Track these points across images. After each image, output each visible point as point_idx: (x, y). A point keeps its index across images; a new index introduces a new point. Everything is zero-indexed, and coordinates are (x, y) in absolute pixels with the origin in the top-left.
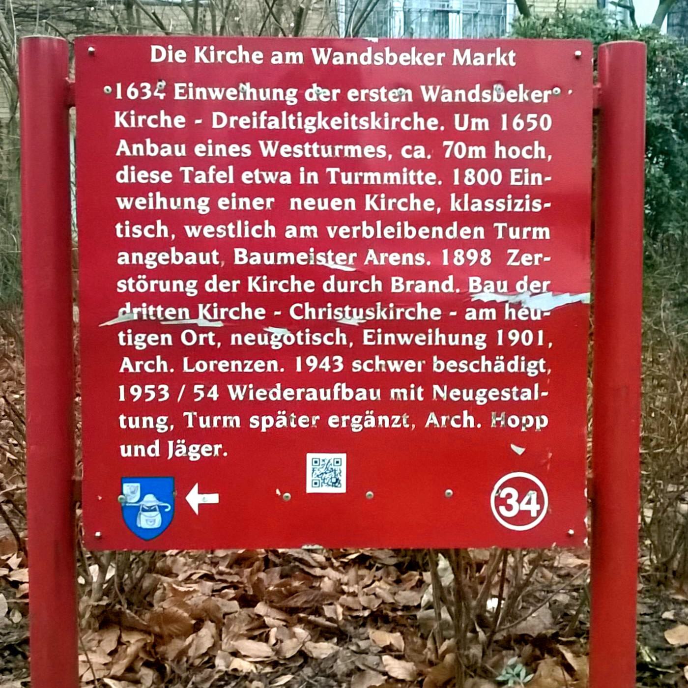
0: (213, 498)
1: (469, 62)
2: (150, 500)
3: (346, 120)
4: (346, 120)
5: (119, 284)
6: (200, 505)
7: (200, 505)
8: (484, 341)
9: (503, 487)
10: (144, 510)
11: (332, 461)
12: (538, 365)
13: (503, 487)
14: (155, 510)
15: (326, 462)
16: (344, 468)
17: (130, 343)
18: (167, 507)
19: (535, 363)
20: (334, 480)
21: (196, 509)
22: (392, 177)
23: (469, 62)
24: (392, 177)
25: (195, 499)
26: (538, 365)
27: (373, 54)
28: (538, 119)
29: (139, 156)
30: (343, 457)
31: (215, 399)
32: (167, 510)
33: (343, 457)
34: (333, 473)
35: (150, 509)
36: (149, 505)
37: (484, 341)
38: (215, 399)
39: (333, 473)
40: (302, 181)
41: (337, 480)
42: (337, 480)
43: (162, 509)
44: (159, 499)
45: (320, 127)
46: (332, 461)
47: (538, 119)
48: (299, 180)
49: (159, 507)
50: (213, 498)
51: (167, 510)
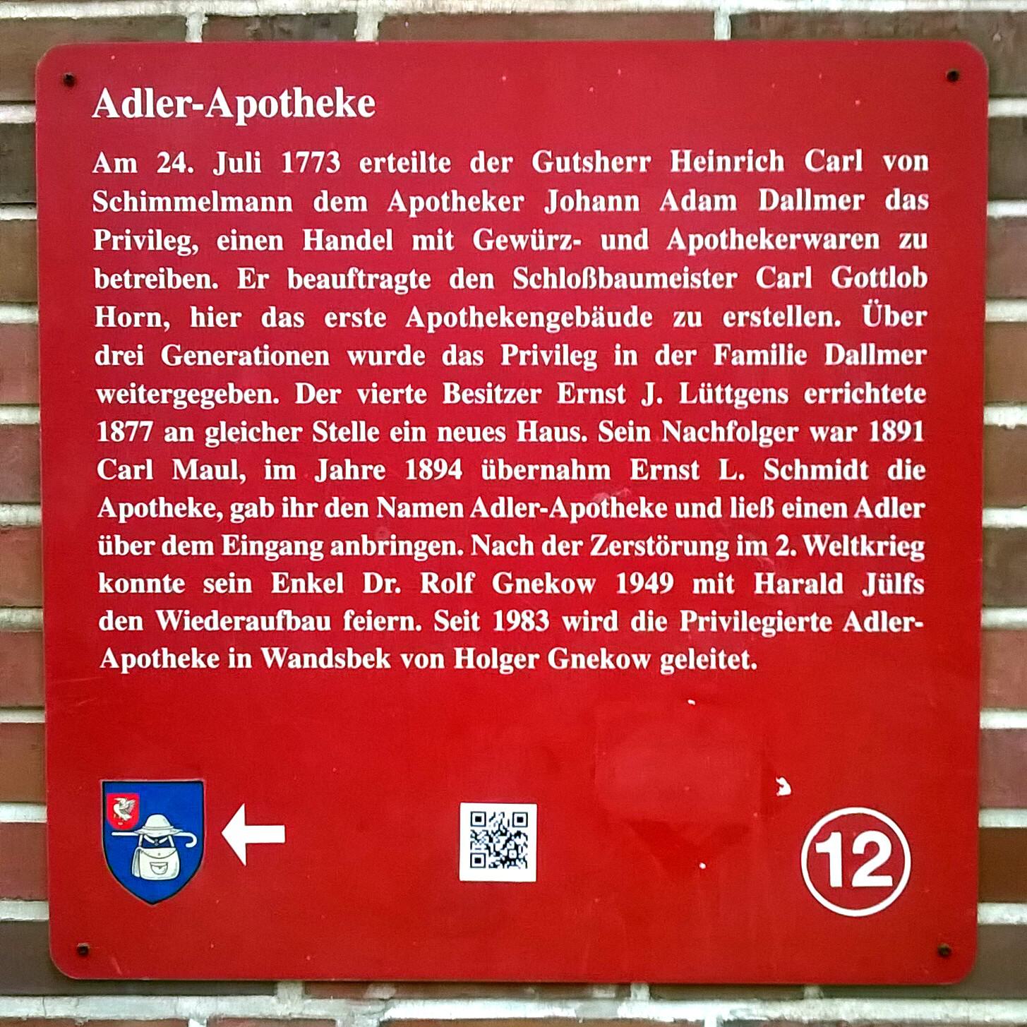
0: (274, 834)
1: (194, 476)
2: (157, 825)
3: (713, 657)
4: (713, 657)
5: (926, 204)
6: (250, 848)
7: (250, 848)
9: (886, 892)
10: (146, 845)
13: (886, 892)
14: (167, 845)
16: (531, 830)
18: (190, 840)
21: (242, 855)
23: (194, 476)
25: (240, 834)
27: (334, 655)
29: (868, 343)
30: (531, 810)
31: (458, 477)
32: (189, 845)
33: (531, 810)
35: (159, 843)
36: (156, 834)
38: (458, 477)
40: (232, 665)
43: (179, 843)
44: (175, 824)
45: (223, 439)
49: (175, 838)
50: (274, 834)
51: (189, 845)
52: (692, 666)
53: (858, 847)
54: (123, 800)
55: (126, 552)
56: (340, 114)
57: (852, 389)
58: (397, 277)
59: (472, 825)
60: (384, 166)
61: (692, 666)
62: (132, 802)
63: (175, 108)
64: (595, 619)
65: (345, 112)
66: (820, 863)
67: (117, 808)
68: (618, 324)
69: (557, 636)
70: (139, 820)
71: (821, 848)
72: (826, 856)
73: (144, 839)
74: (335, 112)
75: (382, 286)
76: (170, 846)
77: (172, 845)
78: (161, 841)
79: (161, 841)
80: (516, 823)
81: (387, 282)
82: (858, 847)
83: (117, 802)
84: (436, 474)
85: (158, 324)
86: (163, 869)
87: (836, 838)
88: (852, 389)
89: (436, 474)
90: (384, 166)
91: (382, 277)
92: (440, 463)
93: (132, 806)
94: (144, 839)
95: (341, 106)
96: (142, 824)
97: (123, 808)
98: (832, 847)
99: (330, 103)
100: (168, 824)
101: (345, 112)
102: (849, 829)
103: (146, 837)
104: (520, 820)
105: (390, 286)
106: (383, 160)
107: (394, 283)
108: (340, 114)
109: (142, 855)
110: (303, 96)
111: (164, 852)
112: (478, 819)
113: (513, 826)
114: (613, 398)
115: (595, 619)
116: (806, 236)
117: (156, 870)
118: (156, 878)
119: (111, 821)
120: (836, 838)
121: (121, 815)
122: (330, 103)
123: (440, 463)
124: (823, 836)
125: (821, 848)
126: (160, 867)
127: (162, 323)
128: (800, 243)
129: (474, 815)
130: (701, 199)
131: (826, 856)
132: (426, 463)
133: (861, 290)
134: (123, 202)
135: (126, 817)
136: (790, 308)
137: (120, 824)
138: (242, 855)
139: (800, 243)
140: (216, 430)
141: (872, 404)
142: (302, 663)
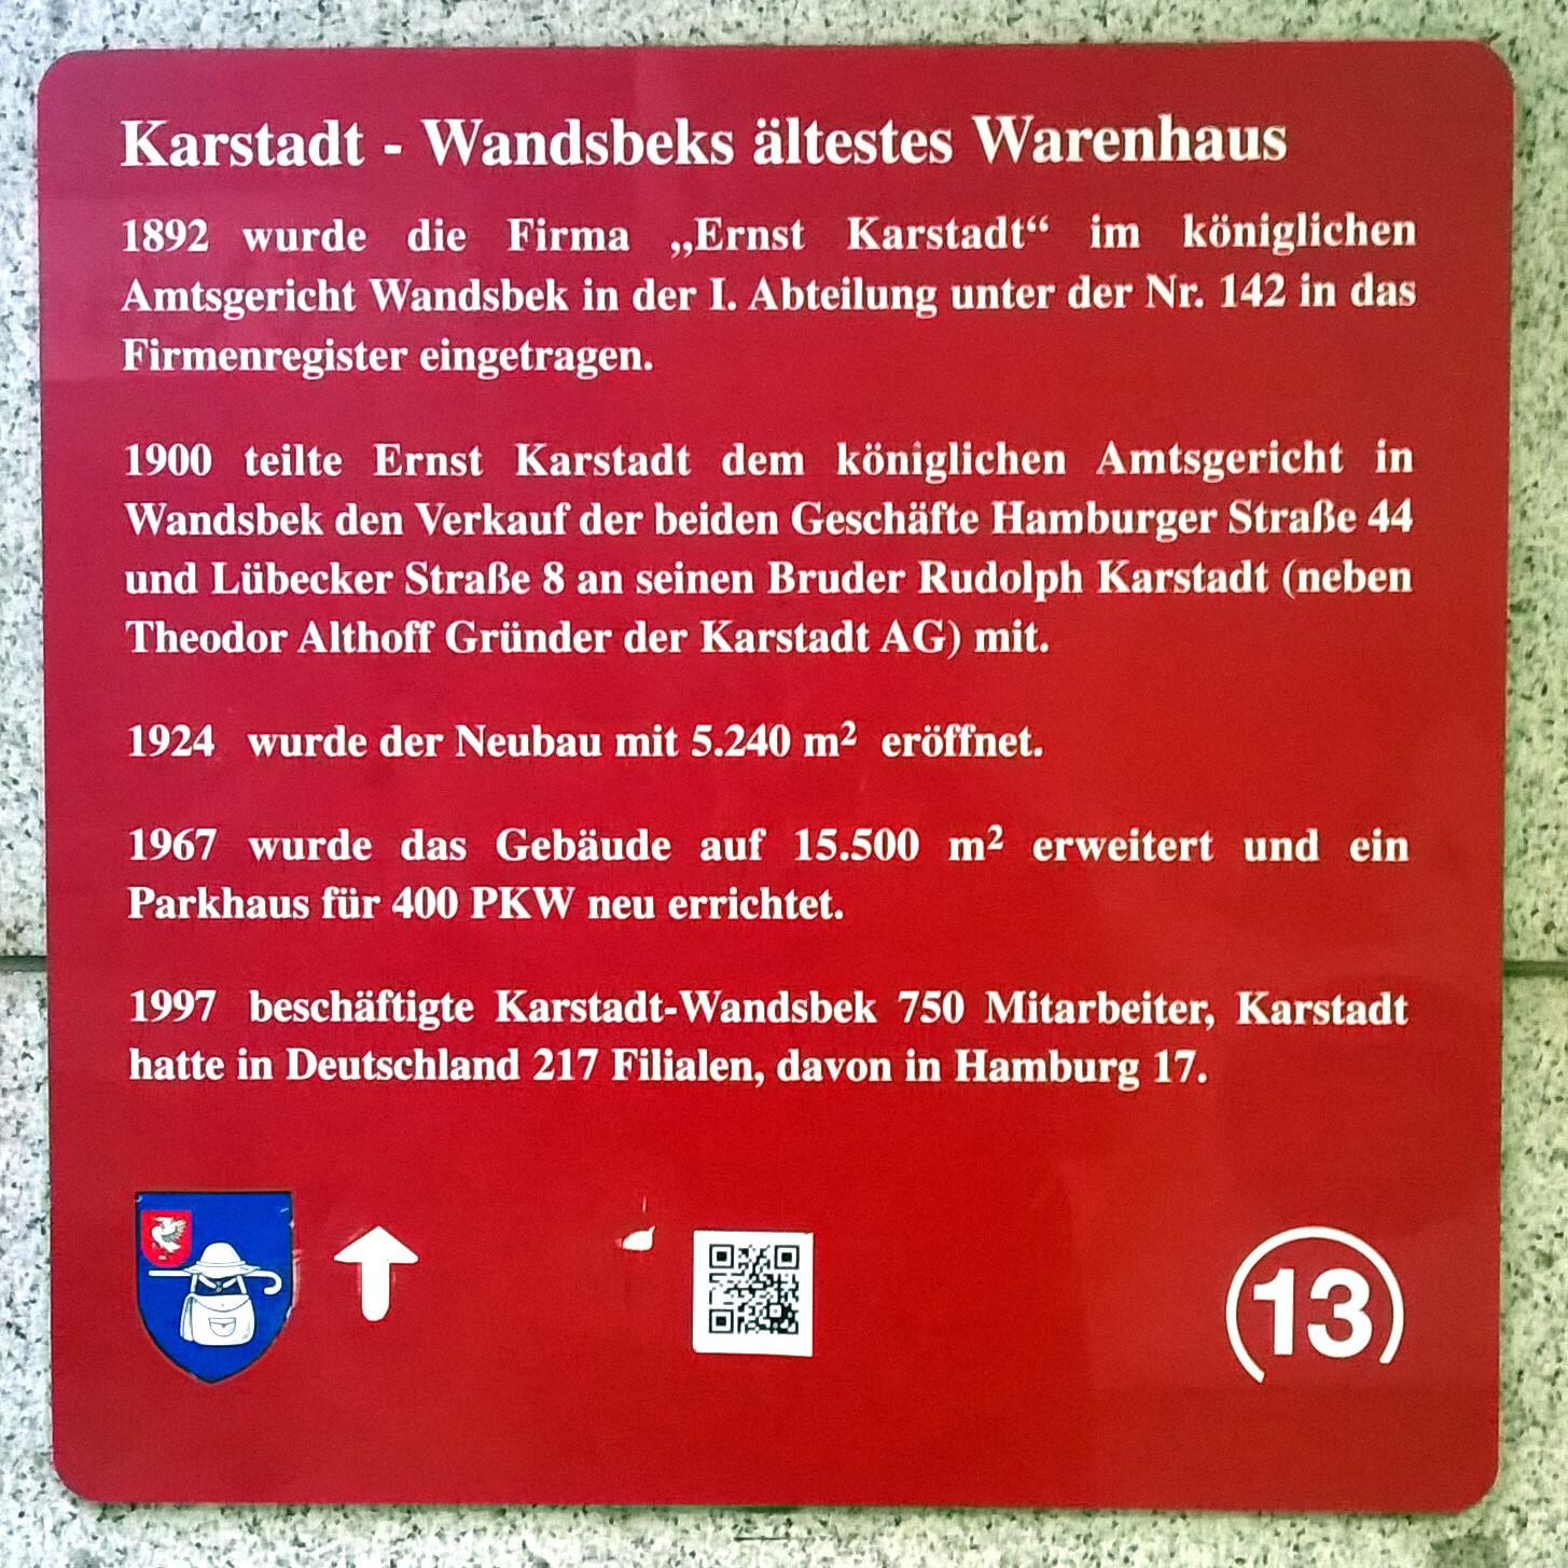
0: (375, 1302)
2: (220, 1260)
6: (353, 1270)
8: (1136, 1075)
10: (203, 1290)
11: (770, 1254)
12: (440, 1006)
14: (235, 1290)
15: (753, 1255)
17: (412, 1017)
18: (271, 1282)
19: (434, 1004)
20: (776, 1312)
22: (226, 522)
24: (226, 522)
26: (440, 1006)
28: (940, 1001)
30: (805, 1242)
32: (269, 1291)
33: (805, 1242)
34: (772, 1291)
37: (1136, 1075)
39: (772, 1291)
41: (786, 1310)
42: (786, 1310)
43: (255, 1287)
44: (246, 1256)
46: (770, 1254)
47: (940, 1001)
48: (905, 1074)
50: (375, 1302)
51: (269, 1291)
53: (1320, 1290)
54: (166, 1221)
55: (267, 1016)
56: (683, 159)
57: (1281, 451)
58: (581, 354)
59: (711, 1266)
62: (181, 1224)
65: (690, 156)
66: (1257, 1317)
67: (157, 1233)
70: (191, 1251)
71: (1261, 1292)
72: (1269, 1305)
73: (199, 1282)
74: (676, 157)
75: (558, 366)
76: (240, 1293)
77: (244, 1290)
78: (226, 1285)
79: (226, 1285)
80: (780, 1263)
81: (565, 361)
82: (1320, 1290)
83: (158, 1224)
84: (169, 242)
87: (1286, 1277)
88: (1281, 451)
89: (169, 242)
91: (558, 353)
92: (175, 226)
93: (180, 1230)
94: (199, 1282)
95: (684, 148)
97: (167, 1232)
98: (1280, 1290)
99: (668, 143)
100: (237, 1258)
101: (690, 156)
102: (1308, 1261)
103: (202, 1279)
104: (787, 1257)
105: (570, 367)
107: (576, 362)
110: (626, 131)
112: (722, 1257)
113: (776, 1267)
117: (218, 1329)
119: (146, 1254)
120: (1286, 1277)
121: (163, 1244)
122: (668, 143)
123: (175, 226)
124: (1264, 1272)
125: (1261, 1292)
129: (715, 1250)
130: (1381, 288)
131: (1269, 1305)
132: (154, 226)
133: (1106, 126)
134: (760, 904)
135: (172, 1247)
137: (163, 1258)
141: (1315, 474)
142: (472, 1072)
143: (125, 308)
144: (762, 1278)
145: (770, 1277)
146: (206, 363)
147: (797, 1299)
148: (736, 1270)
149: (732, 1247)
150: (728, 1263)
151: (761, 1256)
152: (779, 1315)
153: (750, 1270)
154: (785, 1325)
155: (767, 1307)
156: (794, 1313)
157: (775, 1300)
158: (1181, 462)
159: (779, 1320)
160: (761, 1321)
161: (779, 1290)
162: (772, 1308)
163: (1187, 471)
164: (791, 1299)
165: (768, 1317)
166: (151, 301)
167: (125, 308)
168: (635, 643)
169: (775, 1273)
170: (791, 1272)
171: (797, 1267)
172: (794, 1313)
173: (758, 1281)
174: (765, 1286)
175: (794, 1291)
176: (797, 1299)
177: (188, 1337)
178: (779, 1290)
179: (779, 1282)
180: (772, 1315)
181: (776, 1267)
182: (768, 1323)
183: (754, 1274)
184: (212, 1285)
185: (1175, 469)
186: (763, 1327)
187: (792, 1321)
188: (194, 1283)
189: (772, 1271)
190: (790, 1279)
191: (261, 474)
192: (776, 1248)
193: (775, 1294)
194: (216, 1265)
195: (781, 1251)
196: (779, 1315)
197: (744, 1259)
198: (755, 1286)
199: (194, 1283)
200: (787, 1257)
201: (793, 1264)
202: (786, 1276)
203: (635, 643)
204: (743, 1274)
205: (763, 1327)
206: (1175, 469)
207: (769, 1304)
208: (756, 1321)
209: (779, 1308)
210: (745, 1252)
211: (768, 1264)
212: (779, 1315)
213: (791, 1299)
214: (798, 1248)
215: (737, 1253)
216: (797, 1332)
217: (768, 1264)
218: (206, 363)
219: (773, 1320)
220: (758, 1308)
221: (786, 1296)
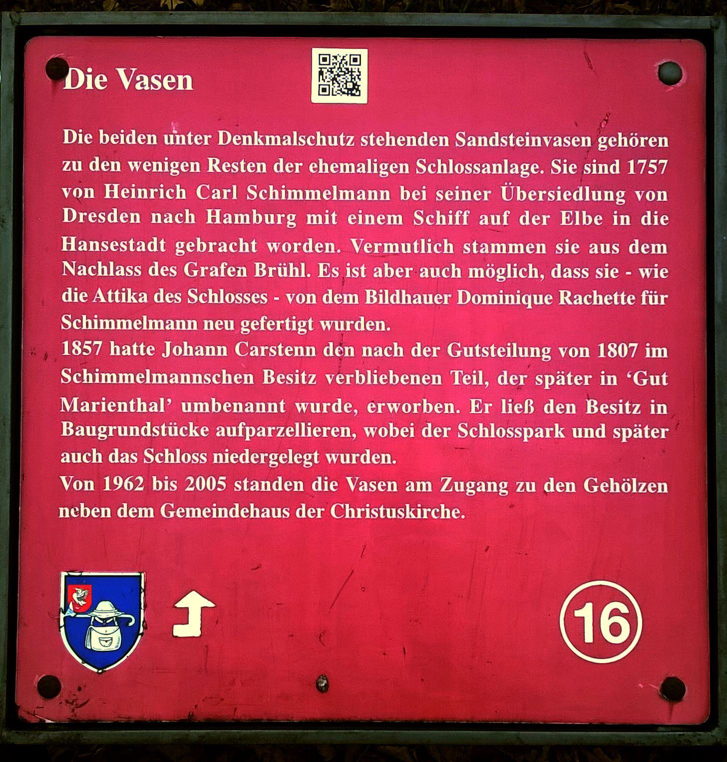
6: (186, 610)
7: (186, 610)
11: (347, 58)
14: (112, 624)
15: (339, 59)
20: (350, 85)
21: (179, 605)
32: (131, 624)
35: (105, 623)
36: (104, 616)
41: (355, 85)
42: (355, 85)
43: (122, 624)
44: (117, 607)
46: (347, 58)
51: (131, 624)
52: (291, 462)
54: (80, 591)
56: (191, 435)
60: (283, 326)
61: (291, 462)
63: (316, 513)
64: (425, 511)
68: (176, 434)
69: (344, 495)
73: (95, 619)
76: (115, 625)
78: (108, 622)
79: (108, 622)
80: (352, 63)
83: (76, 591)
85: (348, 435)
86: (108, 642)
90: (283, 326)
94: (95, 619)
96: (93, 607)
103: (96, 618)
106: (282, 322)
108: (191, 435)
109: (93, 632)
111: (110, 629)
114: (158, 433)
115: (425, 511)
116: (389, 405)
117: (103, 643)
118: (103, 649)
126: (106, 641)
127: (351, 434)
128: (385, 409)
136: (297, 425)
138: (179, 605)
139: (385, 409)
140: (503, 270)
143: (94, 301)
144: (343, 70)
145: (347, 69)
146: (127, 326)
147: (360, 79)
148: (331, 66)
149: (329, 55)
150: (328, 63)
151: (343, 59)
152: (351, 87)
153: (338, 66)
154: (354, 92)
155: (346, 84)
156: (359, 86)
157: (349, 80)
158: (480, 352)
159: (351, 90)
160: (343, 90)
161: (351, 75)
162: (348, 84)
163: (483, 356)
164: (357, 79)
165: (346, 88)
166: (106, 297)
167: (94, 301)
168: (301, 514)
169: (350, 67)
170: (357, 67)
171: (360, 65)
172: (359, 86)
173: (341, 71)
174: (345, 73)
175: (358, 76)
176: (360, 79)
177: (89, 647)
178: (351, 75)
179: (352, 72)
180: (348, 87)
181: (350, 65)
182: (346, 91)
183: (340, 68)
184: (102, 622)
185: (478, 355)
186: (344, 93)
187: (357, 90)
188: (92, 620)
189: (348, 66)
190: (356, 70)
191: (147, 355)
192: (350, 55)
193: (350, 77)
194: (102, 612)
195: (352, 57)
196: (351, 87)
197: (335, 61)
198: (340, 73)
199: (92, 620)
200: (355, 60)
201: (358, 63)
202: (355, 68)
203: (301, 514)
204: (334, 68)
205: (344, 93)
206: (478, 355)
207: (347, 82)
208: (341, 90)
209: (351, 84)
210: (335, 57)
211: (346, 63)
212: (351, 87)
213: (357, 79)
214: (360, 55)
215: (332, 58)
216: (359, 95)
217: (346, 63)
218: (127, 326)
219: (349, 89)
220: (342, 84)
221: (355, 79)
